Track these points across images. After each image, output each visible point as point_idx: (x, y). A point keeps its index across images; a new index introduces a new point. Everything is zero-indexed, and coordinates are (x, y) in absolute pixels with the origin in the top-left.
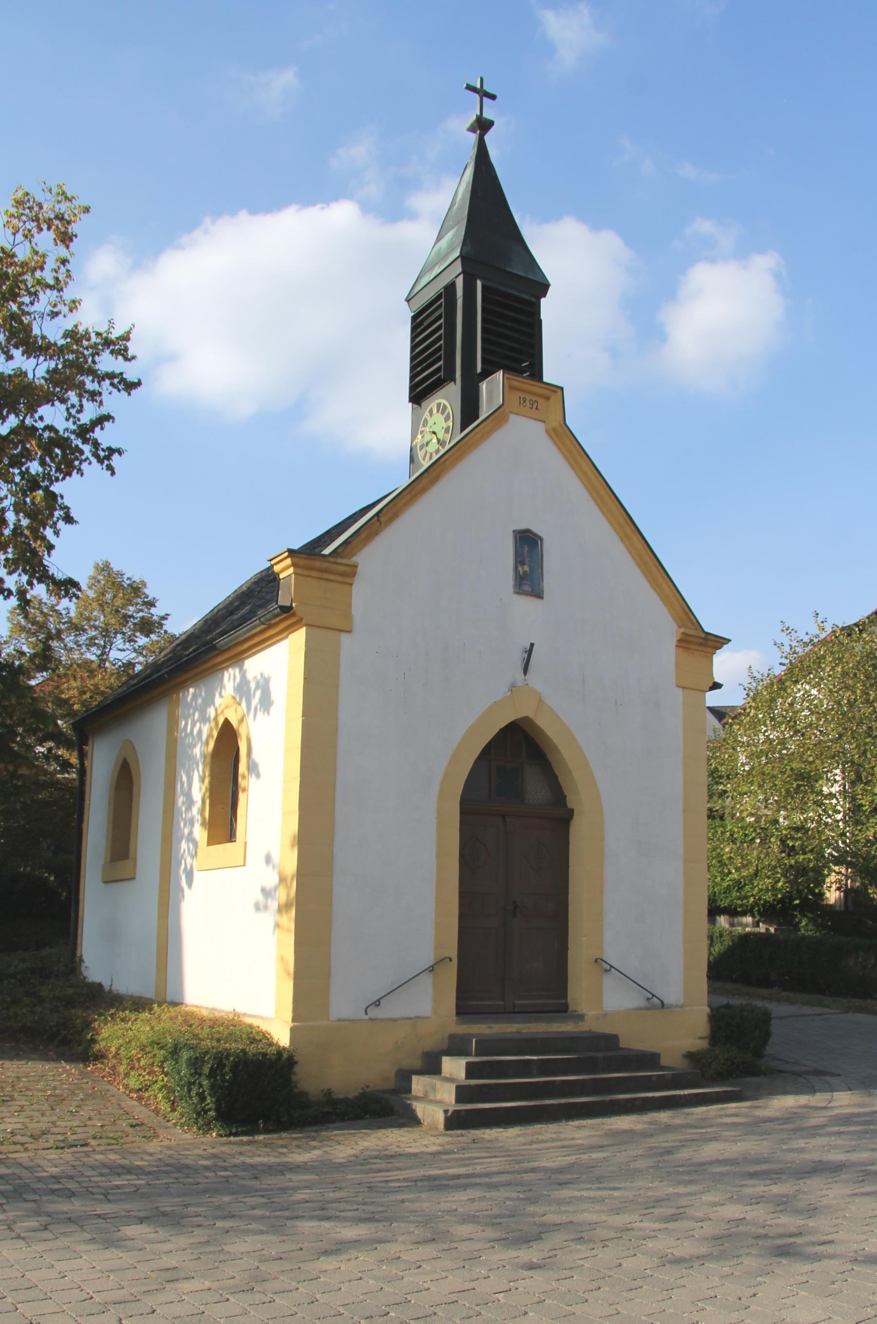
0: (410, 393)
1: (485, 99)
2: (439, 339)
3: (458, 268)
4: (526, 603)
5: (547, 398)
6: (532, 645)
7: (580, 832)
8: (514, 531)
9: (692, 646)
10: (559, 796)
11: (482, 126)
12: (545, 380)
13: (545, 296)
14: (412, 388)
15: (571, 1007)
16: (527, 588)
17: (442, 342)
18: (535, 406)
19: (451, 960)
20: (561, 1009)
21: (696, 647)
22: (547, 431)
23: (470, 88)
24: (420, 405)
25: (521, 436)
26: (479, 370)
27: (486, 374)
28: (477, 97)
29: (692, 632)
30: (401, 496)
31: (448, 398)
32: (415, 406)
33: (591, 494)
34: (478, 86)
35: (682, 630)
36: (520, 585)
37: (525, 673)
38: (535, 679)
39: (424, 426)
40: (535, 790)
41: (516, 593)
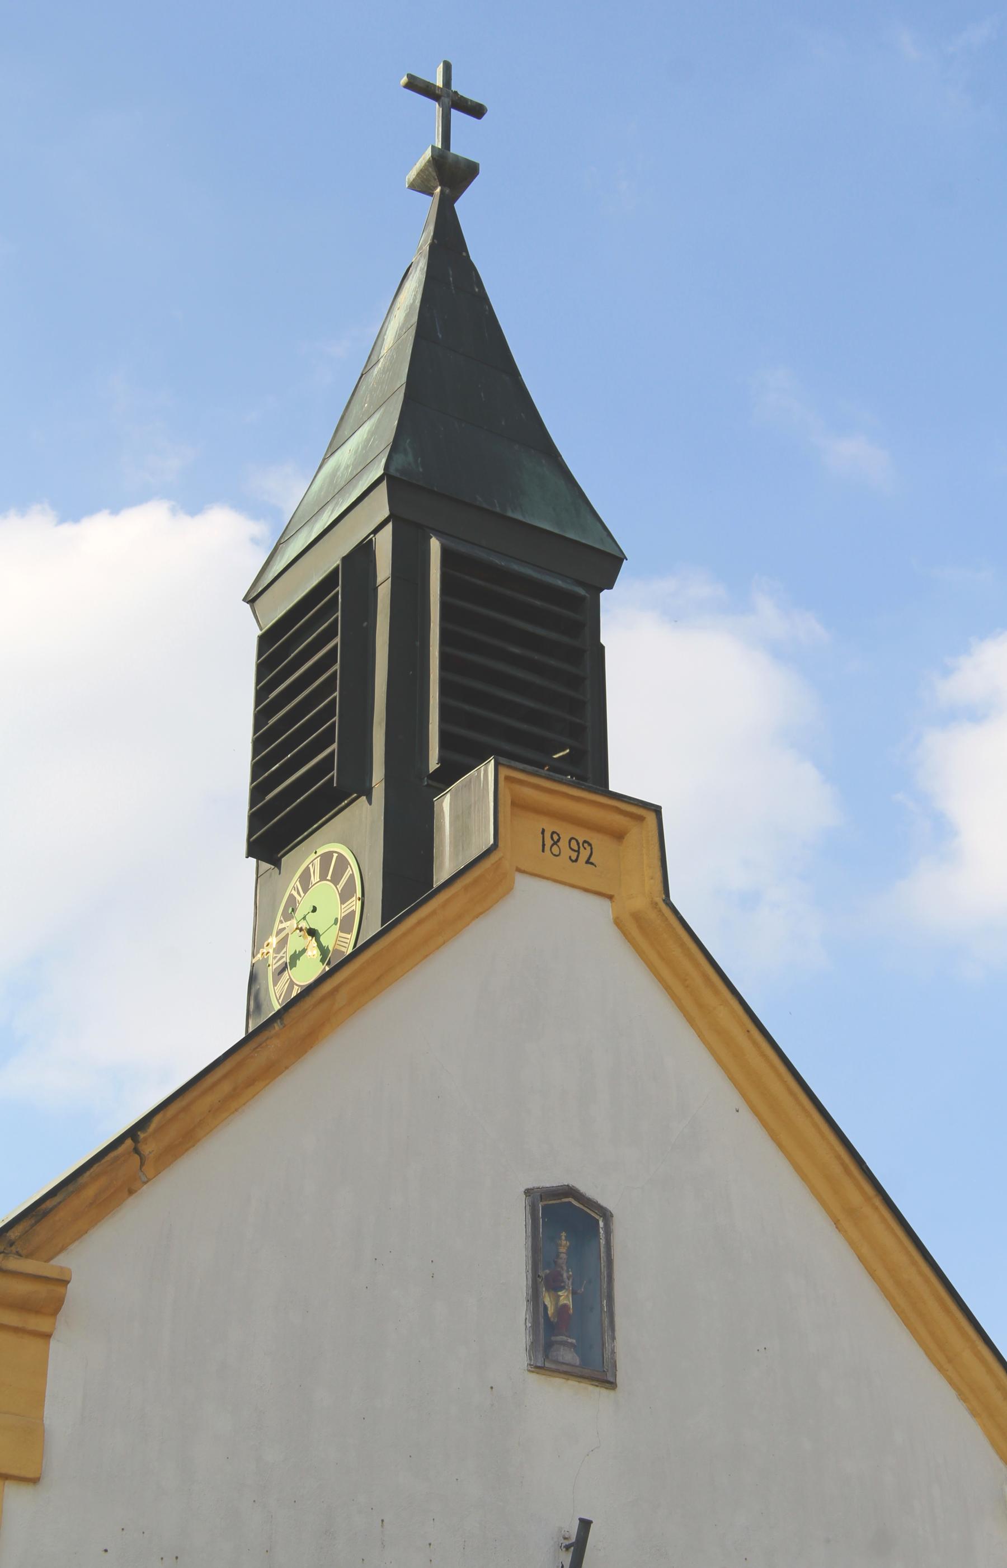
0: (251, 833)
1: (454, 112)
2: (329, 686)
3: (380, 506)
4: (561, 1404)
5: (619, 836)
6: (585, 1525)
8: (528, 1192)
11: (449, 175)
12: (613, 787)
13: (610, 586)
14: (256, 820)
16: (569, 1356)
17: (338, 640)
18: (584, 854)
22: (618, 922)
23: (415, 85)
24: (276, 863)
25: (544, 929)
26: (433, 764)
27: (450, 773)
28: (437, 109)
30: (210, 1080)
31: (350, 841)
32: (265, 866)
33: (744, 1095)
34: (439, 82)
36: (548, 1346)
39: (287, 916)
41: (537, 1369)
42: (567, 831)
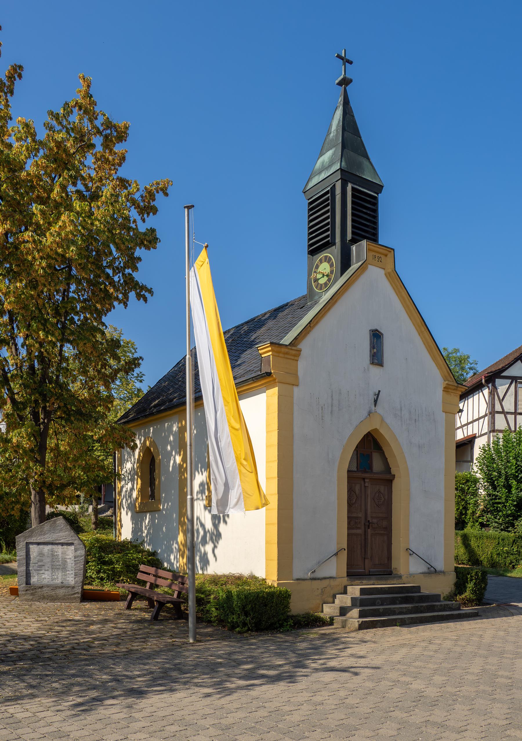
3: (338, 176)
4: (375, 370)
6: (379, 391)
7: (396, 484)
9: (450, 390)
10: (388, 469)
12: (380, 242)
15: (394, 572)
16: (376, 361)
19: (345, 550)
20: (387, 572)
21: (452, 391)
22: (385, 274)
23: (339, 56)
27: (354, 241)
29: (451, 383)
31: (333, 253)
34: (343, 55)
35: (447, 382)
37: (375, 406)
38: (379, 409)
40: (377, 465)
42: (377, 255)
